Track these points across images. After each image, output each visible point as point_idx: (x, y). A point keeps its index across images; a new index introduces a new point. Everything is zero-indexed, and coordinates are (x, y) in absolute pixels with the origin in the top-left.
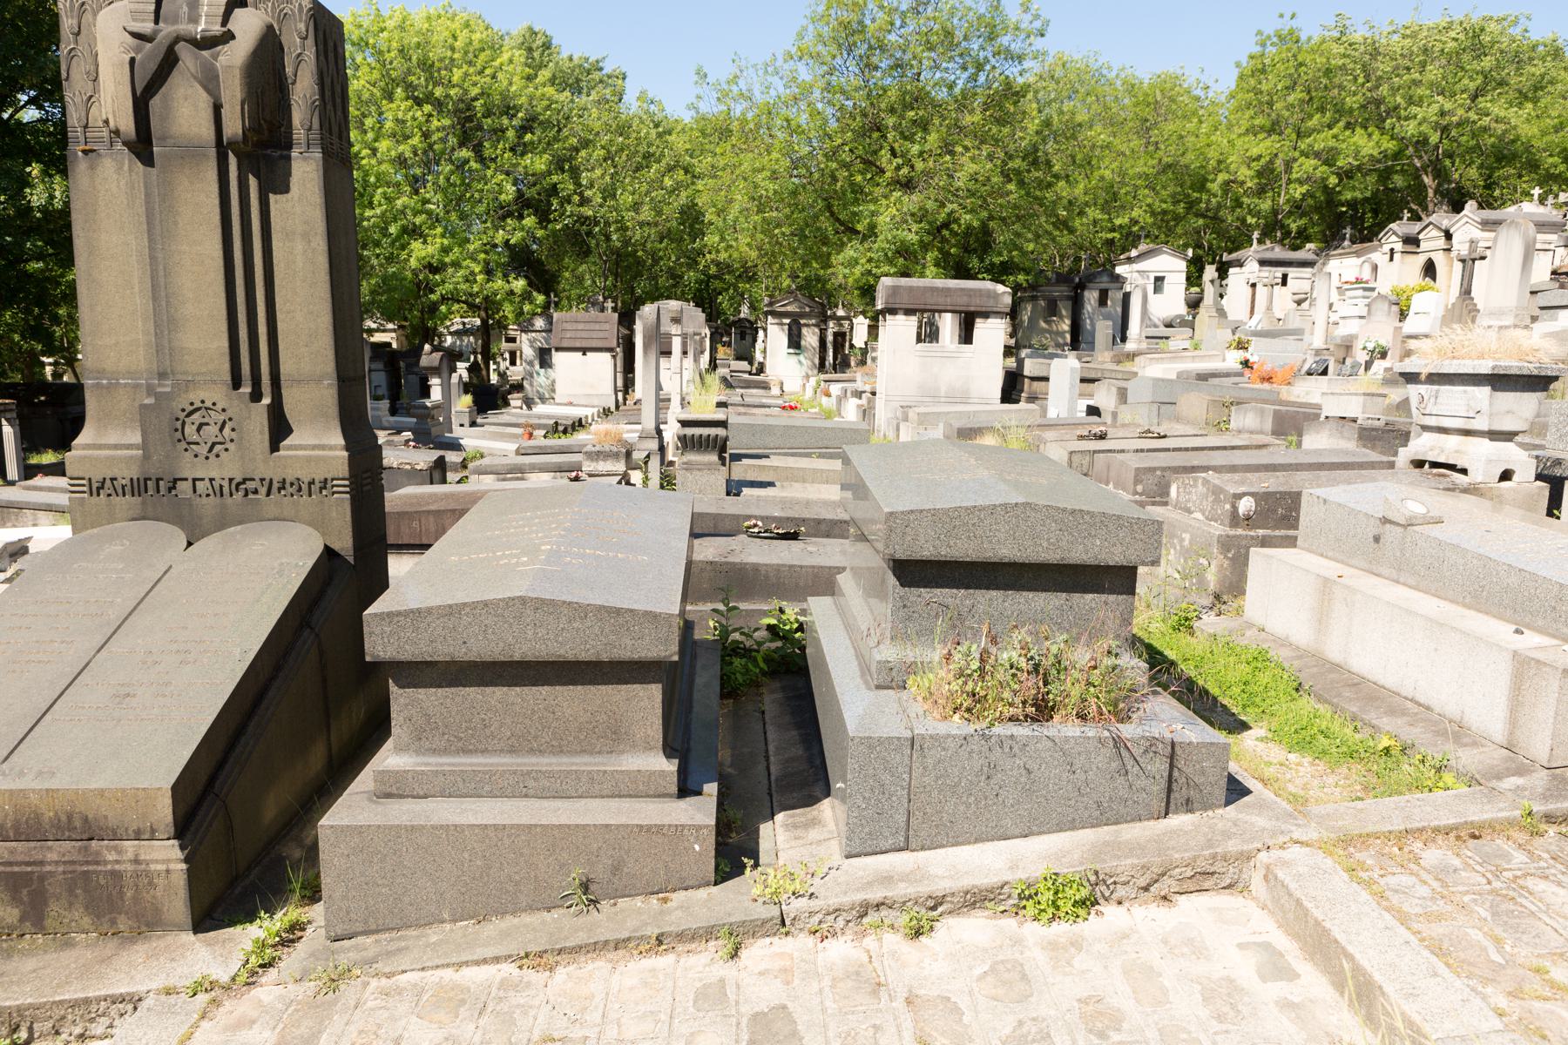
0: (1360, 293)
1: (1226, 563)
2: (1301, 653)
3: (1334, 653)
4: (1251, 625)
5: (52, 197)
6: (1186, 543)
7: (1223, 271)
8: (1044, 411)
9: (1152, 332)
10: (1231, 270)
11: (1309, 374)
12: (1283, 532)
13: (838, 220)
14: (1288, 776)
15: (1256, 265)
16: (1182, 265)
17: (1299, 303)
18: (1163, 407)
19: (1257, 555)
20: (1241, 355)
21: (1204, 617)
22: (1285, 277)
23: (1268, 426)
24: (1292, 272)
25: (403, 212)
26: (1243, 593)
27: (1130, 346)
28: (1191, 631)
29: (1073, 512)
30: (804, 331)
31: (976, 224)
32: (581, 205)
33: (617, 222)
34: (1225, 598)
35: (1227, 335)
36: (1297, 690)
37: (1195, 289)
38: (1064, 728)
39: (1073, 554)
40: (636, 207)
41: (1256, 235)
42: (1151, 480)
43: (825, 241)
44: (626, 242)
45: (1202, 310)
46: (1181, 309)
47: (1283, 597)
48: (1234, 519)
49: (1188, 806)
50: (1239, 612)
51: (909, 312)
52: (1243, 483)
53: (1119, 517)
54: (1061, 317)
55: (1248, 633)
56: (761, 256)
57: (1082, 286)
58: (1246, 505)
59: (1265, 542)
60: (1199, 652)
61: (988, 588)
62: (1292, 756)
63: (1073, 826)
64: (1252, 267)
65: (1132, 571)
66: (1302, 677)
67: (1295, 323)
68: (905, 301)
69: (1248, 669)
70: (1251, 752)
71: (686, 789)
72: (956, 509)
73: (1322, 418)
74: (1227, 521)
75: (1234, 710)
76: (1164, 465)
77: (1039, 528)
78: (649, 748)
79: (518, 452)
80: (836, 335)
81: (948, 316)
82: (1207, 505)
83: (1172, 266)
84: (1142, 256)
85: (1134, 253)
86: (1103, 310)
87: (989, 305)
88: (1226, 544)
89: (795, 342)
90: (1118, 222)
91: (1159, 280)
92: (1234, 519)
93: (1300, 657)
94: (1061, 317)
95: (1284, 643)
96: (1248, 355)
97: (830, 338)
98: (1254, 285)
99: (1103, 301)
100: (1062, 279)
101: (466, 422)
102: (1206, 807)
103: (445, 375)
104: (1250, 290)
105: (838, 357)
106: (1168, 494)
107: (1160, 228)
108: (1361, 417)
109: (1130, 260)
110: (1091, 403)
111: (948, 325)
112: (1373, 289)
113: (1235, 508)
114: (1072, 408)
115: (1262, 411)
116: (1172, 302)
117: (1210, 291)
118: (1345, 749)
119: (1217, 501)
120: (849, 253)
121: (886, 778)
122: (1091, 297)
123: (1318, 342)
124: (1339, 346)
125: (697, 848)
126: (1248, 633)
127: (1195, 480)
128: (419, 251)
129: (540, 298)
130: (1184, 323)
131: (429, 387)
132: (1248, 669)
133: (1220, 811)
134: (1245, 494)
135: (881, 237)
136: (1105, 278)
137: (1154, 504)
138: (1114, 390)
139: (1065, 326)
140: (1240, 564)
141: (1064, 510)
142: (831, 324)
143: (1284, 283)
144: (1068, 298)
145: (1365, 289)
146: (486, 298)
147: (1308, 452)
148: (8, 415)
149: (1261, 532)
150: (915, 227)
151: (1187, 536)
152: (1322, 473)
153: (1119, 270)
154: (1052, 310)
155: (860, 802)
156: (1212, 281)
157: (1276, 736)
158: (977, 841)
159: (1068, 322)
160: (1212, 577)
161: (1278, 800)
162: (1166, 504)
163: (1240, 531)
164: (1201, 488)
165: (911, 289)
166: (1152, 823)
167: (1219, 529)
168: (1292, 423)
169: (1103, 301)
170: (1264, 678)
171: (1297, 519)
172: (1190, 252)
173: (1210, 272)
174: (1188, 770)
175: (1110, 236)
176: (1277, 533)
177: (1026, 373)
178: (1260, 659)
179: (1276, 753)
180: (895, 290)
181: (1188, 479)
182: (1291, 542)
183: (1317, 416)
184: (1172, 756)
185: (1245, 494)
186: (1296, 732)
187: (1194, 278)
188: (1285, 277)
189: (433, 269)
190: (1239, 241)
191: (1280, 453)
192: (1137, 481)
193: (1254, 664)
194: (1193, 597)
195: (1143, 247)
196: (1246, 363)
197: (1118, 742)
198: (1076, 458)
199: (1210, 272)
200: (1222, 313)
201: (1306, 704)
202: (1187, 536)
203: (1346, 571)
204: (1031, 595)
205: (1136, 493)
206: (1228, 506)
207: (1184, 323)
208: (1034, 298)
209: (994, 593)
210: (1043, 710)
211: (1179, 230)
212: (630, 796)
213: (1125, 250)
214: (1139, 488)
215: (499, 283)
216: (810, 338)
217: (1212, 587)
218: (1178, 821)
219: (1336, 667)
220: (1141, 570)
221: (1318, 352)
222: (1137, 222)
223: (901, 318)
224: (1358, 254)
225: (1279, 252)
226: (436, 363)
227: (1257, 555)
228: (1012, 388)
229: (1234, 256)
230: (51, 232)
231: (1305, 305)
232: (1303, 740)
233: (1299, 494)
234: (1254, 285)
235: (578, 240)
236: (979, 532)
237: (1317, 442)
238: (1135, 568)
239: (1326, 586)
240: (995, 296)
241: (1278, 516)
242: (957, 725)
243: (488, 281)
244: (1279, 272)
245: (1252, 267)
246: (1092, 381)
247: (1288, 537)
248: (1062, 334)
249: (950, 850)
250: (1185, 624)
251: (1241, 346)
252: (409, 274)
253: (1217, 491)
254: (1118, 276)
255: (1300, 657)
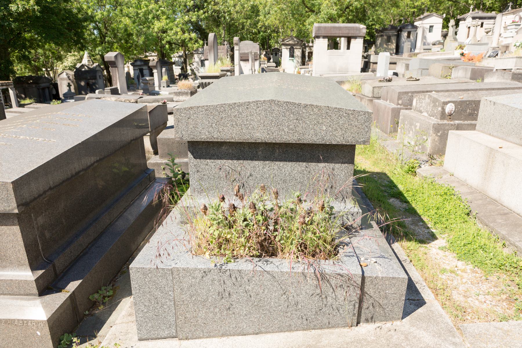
0: (514, 27)
1: (437, 138)
2: (473, 191)
3: (493, 192)
4: (446, 172)
5: (18, 7)
6: (418, 128)
7: (457, 25)
8: (375, 75)
9: (426, 47)
10: (461, 22)
11: (489, 57)
12: (469, 122)
13: (307, 7)
14: (455, 283)
15: (471, 19)
16: (441, 21)
17: (487, 33)
18: (424, 71)
19: (453, 134)
20: (460, 51)
21: (422, 166)
22: (482, 24)
23: (469, 75)
24: (485, 22)
25: (152, 11)
26: (444, 154)
27: (417, 51)
28: (415, 174)
29: (306, 106)
30: (295, 50)
31: (359, 6)
32: (214, 5)
33: (228, 11)
34: (435, 156)
35: (456, 44)
36: (468, 214)
37: (445, 30)
38: (285, 264)
39: (306, 136)
40: (235, 6)
41: (472, 7)
42: (406, 98)
43: (301, 15)
44: (232, 19)
45: (447, 38)
46: (440, 39)
47: (465, 157)
48: (443, 115)
49: (371, 320)
50: (441, 164)
51: (324, 37)
52: (449, 96)
53: (340, 110)
54: (392, 43)
55: (444, 177)
56: (280, 23)
57: (400, 30)
58: (450, 108)
59: (458, 128)
60: (416, 187)
61: (252, 159)
62: (460, 264)
63: (290, 329)
64: (469, 20)
65: (352, 148)
66: (472, 207)
67: (485, 41)
68: (323, 33)
69: (440, 199)
70: (434, 261)
71: (45, 288)
72: (222, 105)
73: (495, 70)
74: (439, 117)
75: (429, 226)
76: (413, 90)
77: (281, 118)
78: (20, 265)
79: (170, 94)
80: (309, 53)
81: (343, 39)
82: (430, 108)
83: (436, 21)
84: (425, 18)
85: (422, 16)
86: (409, 39)
87: (356, 33)
88: (437, 128)
89: (292, 55)
90: (416, 4)
91: (431, 27)
92: (443, 115)
93: (471, 193)
94: (392, 43)
95: (463, 183)
96: (463, 51)
97: (307, 54)
98: (469, 28)
99: (409, 37)
100: (393, 27)
101: (165, 85)
102: (387, 318)
103: (159, 68)
104: (467, 29)
105: (306, 59)
106: (412, 104)
107: (433, 7)
108: (514, 68)
109: (420, 19)
110: (395, 71)
111: (343, 42)
112: (519, 25)
113: (443, 109)
114: (386, 73)
115: (466, 69)
116: (436, 35)
117: (451, 30)
118: (495, 261)
119: (435, 106)
120: (311, 19)
121: (158, 294)
122: (405, 34)
123: (494, 45)
124: (503, 46)
125: (39, 333)
126: (444, 177)
127: (425, 96)
128: (157, 25)
129: (201, 42)
130: (440, 43)
131: (153, 73)
132: (440, 199)
133: (398, 323)
134: (449, 102)
135: (322, 13)
136: (410, 27)
137: (406, 109)
138: (404, 65)
139: (394, 46)
140: (443, 139)
141: (299, 105)
142: (307, 49)
143: (482, 26)
144: (395, 35)
145: (516, 25)
146: (182, 40)
147: (487, 84)
148: (11, 87)
149: (457, 122)
150: (335, 8)
151: (418, 124)
152: (493, 91)
153: (415, 24)
154: (389, 40)
155: (142, 308)
156: (452, 26)
157: (451, 247)
158: (223, 335)
159: (395, 45)
160: (429, 146)
161: (443, 312)
162: (411, 109)
163: (445, 122)
164: (427, 100)
165: (325, 28)
166: (346, 330)
167: (434, 121)
168: (478, 74)
169: (409, 37)
170: (448, 207)
171: (477, 115)
172: (444, 15)
173: (452, 22)
174: (376, 296)
175: (413, 10)
176: (466, 122)
177: (371, 61)
178: (448, 194)
179: (450, 261)
180: (319, 28)
181: (421, 96)
182: (473, 127)
183: (492, 70)
184: (362, 288)
185: (449, 102)
186: (464, 245)
187: (445, 26)
188: (482, 24)
189: (164, 31)
190: (465, 10)
191: (474, 85)
192: (399, 99)
193: (445, 196)
194: (419, 156)
195: (426, 14)
196: (462, 54)
197: (322, 277)
198: (376, 90)
199: (452, 22)
200: (455, 39)
201: (472, 227)
202: (418, 124)
203: (504, 144)
204: (281, 164)
205: (398, 104)
206: (440, 109)
207: (440, 43)
208: (382, 36)
209: (256, 163)
210: (267, 249)
211: (441, 8)
212: (10, 294)
213: (418, 16)
214: (400, 102)
215: (186, 35)
216: (298, 52)
217: (428, 151)
218: (365, 328)
219: (494, 201)
220: (359, 149)
221: (494, 48)
222: (424, 4)
223: (321, 40)
224: (513, 13)
225: (481, 14)
226: (155, 64)
227: (453, 134)
228: (366, 68)
229: (462, 16)
230: (22, 20)
231: (490, 34)
232: (467, 252)
233: (479, 102)
234: (469, 28)
235: (216, 20)
236: (239, 122)
237: (490, 80)
238: (355, 145)
239: (491, 152)
240: (359, 29)
241: (467, 113)
242: (206, 261)
243: (182, 35)
244: (480, 22)
245: (469, 20)
246: (395, 63)
247: (471, 124)
248: (392, 50)
249: (205, 340)
250: (412, 171)
251: (461, 48)
252: (155, 34)
253: (435, 101)
254: (416, 26)
255: (471, 193)
